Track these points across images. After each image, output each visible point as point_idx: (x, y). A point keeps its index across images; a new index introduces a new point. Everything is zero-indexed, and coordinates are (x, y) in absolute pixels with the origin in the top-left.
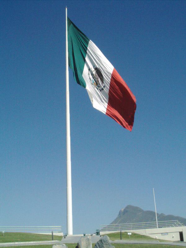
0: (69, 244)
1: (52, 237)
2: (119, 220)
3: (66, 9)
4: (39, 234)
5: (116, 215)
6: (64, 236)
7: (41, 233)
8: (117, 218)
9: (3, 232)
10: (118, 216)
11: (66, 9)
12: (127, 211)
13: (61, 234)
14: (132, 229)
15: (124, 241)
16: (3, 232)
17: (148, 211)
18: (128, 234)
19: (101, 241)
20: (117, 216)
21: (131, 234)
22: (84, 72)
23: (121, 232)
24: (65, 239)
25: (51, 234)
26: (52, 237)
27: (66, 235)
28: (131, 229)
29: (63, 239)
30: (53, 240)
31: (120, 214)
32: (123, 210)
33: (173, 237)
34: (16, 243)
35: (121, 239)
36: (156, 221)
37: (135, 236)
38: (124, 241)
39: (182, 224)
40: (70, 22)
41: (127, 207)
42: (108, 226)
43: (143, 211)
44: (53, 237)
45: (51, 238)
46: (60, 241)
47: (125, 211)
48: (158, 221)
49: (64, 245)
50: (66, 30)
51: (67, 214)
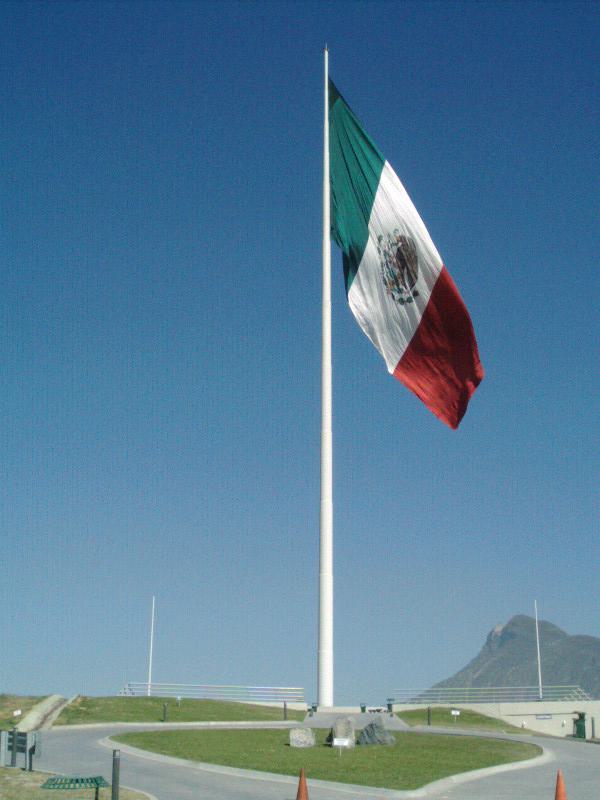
0: (318, 729)
1: (285, 715)
2: (486, 665)
3: (326, 53)
4: (252, 705)
5: (476, 648)
6: (309, 710)
7: (257, 703)
8: (480, 657)
9: (179, 698)
10: (484, 647)
11: (326, 53)
12: (512, 635)
13: (304, 706)
14: (470, 702)
15: (436, 728)
16: (179, 698)
17: (579, 637)
18: (453, 713)
19: (371, 726)
20: (480, 649)
21: (458, 713)
22: (365, 254)
23: (285, 709)
24: (312, 719)
25: (281, 705)
26: (285, 715)
27: (315, 709)
28: (464, 702)
29: (307, 719)
30: (285, 718)
31: (489, 640)
32: (499, 629)
33: (563, 725)
34: (212, 723)
35: (429, 724)
36: (538, 684)
37: (469, 718)
38: (436, 728)
39: (590, 696)
40: (335, 94)
41: (512, 623)
42: (429, 691)
43: (564, 634)
44: (286, 714)
45: (283, 716)
46: (300, 723)
47: (507, 635)
48: (543, 684)
49: (310, 730)
50: (323, 107)
51: (319, 648)
